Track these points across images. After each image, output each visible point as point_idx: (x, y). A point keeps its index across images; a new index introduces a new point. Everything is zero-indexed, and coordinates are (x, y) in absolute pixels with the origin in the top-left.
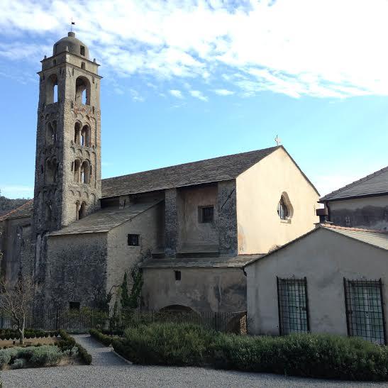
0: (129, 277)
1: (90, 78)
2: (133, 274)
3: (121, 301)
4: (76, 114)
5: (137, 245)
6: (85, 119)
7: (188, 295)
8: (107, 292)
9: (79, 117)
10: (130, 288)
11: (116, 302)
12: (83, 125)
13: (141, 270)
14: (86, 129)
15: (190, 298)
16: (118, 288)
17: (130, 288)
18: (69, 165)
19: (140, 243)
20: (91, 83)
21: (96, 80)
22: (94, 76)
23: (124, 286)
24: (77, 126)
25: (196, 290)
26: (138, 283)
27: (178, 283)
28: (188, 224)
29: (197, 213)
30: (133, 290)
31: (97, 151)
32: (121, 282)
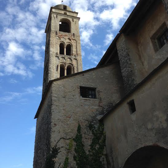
0: (84, 130)
1: (70, 19)
2: (91, 127)
3: (75, 158)
4: (60, 38)
5: (95, 97)
6: (68, 41)
7: (150, 126)
8: (53, 145)
9: (62, 40)
10: (87, 142)
11: (67, 159)
12: (66, 44)
13: (102, 121)
14: (69, 47)
15: (152, 129)
16: (68, 141)
17: (87, 142)
18: (55, 68)
19: (97, 96)
20: (71, 21)
21: (75, 20)
22: (73, 17)
23: (78, 139)
24: (62, 46)
25: (157, 113)
26: (99, 138)
27: (134, 117)
28: (146, 63)
29: (151, 44)
30: (92, 146)
31: (78, 58)
32: (73, 135)
